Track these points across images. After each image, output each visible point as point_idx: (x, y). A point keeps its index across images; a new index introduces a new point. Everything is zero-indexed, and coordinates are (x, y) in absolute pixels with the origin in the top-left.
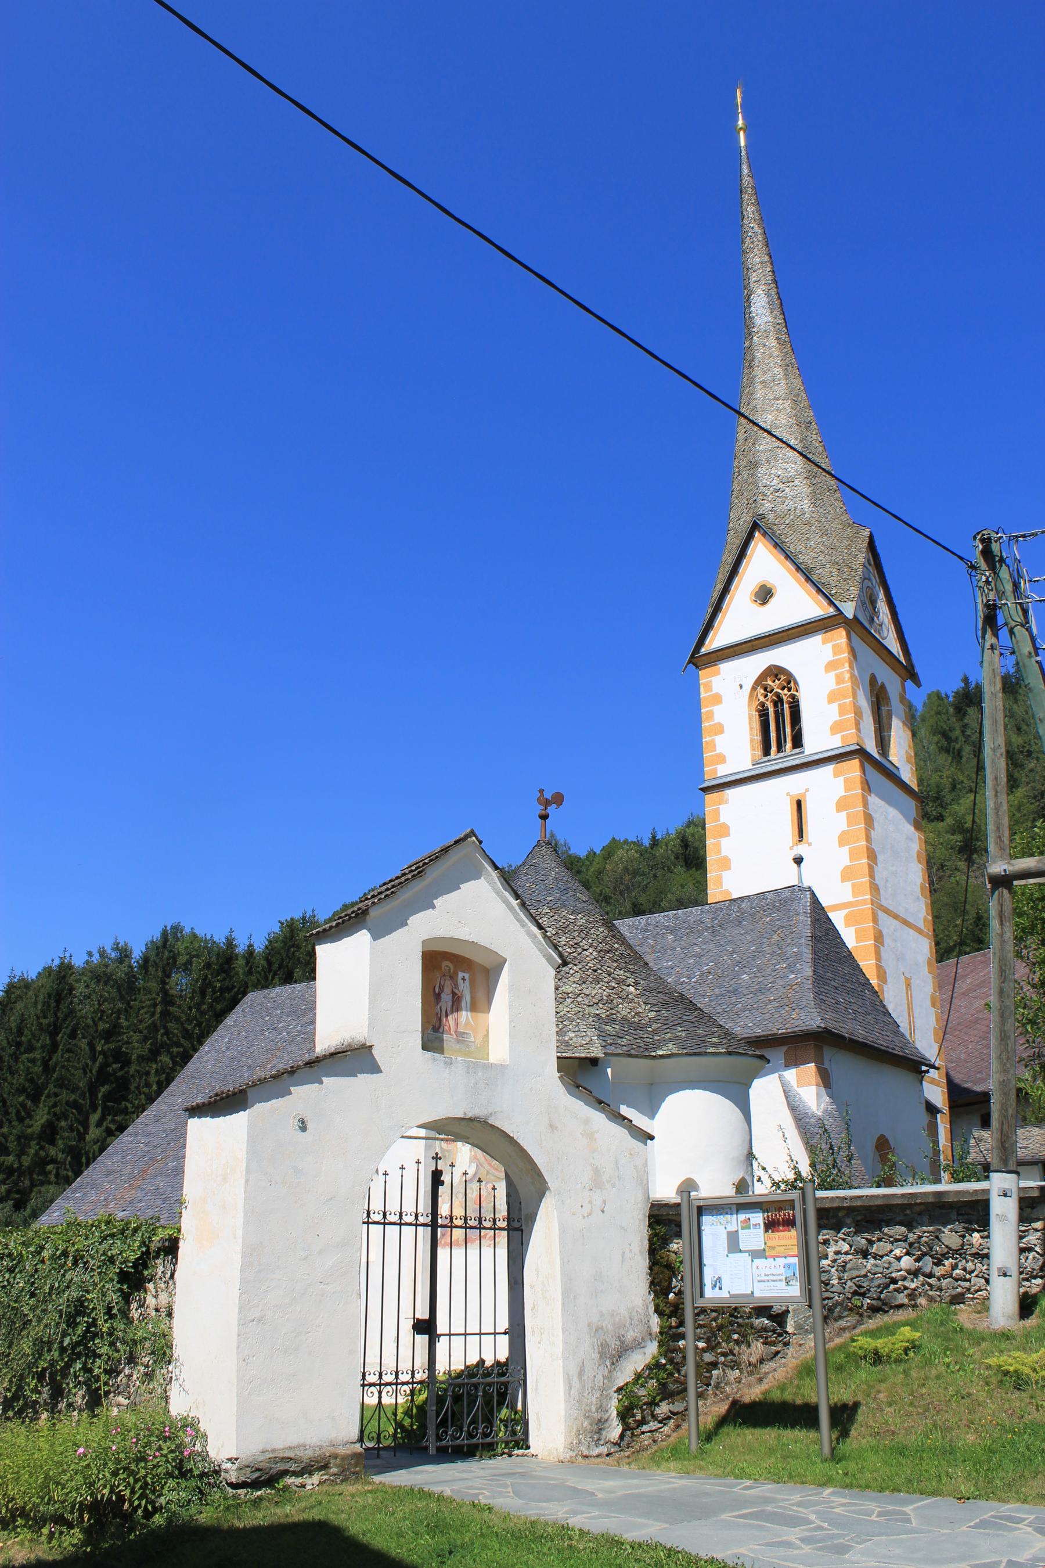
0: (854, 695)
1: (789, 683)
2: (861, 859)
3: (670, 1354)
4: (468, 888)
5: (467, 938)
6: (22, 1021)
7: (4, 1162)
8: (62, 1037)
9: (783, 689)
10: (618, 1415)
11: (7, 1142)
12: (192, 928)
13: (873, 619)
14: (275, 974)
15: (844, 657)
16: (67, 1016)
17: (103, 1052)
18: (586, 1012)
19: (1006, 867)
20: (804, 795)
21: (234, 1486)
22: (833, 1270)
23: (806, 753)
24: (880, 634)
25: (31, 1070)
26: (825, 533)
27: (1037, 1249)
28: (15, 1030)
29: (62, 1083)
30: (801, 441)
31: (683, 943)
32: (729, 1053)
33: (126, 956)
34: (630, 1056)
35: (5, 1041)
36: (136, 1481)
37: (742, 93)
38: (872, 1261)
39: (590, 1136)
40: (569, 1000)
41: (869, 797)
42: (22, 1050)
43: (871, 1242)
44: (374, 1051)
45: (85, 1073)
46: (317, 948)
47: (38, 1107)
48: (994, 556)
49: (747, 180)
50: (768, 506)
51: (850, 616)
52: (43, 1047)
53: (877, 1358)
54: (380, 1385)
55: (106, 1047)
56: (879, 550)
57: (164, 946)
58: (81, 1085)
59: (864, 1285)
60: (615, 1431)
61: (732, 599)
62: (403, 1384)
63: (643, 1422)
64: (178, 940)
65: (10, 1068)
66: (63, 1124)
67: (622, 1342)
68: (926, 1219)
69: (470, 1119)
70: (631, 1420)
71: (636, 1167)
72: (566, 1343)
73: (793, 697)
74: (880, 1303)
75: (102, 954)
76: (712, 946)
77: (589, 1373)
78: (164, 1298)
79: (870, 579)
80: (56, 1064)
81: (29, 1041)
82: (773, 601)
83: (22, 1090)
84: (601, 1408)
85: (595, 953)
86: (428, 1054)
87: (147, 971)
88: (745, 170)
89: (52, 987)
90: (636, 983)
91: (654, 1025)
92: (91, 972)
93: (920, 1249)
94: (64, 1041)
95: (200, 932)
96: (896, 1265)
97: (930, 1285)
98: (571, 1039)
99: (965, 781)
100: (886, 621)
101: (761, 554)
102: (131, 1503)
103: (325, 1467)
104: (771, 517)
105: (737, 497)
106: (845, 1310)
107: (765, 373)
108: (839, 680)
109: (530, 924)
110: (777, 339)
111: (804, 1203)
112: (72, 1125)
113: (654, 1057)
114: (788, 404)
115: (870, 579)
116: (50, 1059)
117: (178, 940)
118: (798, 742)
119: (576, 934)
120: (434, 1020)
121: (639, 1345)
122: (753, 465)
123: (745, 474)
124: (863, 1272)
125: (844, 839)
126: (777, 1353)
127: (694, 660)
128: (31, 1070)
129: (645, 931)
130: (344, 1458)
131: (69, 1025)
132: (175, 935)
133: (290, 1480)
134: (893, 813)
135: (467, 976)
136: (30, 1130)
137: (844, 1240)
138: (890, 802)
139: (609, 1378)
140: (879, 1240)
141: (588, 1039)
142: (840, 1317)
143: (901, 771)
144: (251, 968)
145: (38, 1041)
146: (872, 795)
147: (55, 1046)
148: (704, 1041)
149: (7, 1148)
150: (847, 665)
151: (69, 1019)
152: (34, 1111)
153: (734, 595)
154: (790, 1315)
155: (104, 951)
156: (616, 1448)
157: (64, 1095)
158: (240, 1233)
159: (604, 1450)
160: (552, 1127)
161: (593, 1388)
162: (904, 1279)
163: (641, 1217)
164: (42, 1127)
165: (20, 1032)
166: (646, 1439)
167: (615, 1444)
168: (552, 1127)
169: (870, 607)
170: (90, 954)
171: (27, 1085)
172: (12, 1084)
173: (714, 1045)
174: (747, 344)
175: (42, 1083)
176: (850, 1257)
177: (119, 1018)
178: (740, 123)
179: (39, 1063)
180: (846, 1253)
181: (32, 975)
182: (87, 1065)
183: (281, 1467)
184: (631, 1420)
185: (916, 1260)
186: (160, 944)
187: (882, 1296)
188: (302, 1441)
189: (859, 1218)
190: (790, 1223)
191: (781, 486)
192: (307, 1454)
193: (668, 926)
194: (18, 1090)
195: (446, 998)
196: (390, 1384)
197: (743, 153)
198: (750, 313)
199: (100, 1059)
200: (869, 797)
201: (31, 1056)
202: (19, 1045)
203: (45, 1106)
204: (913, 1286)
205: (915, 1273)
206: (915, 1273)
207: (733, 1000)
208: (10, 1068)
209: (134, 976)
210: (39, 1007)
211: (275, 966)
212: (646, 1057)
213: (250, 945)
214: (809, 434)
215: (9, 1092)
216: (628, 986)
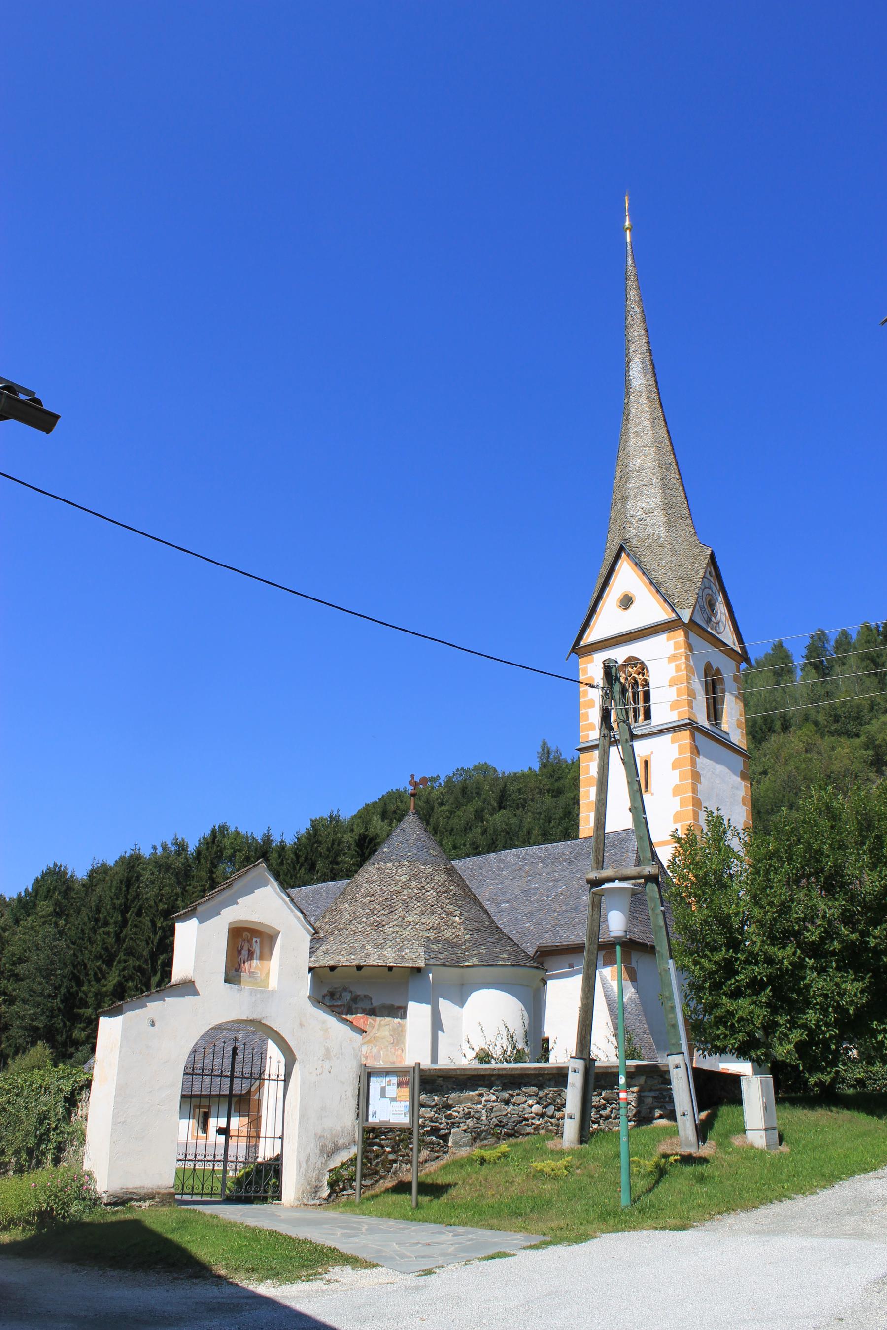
0: (689, 679)
1: (643, 670)
2: (688, 806)
3: (365, 1154)
4: (259, 892)
5: (256, 920)
6: (100, 901)
7: (84, 1013)
8: (131, 915)
9: (638, 675)
10: (328, 1184)
11: (87, 997)
12: (236, 828)
13: (710, 619)
14: (302, 865)
15: (682, 652)
16: (135, 898)
17: (162, 928)
18: (420, 935)
19: (596, 875)
20: (649, 756)
21: (106, 1205)
22: (484, 1111)
23: (652, 725)
24: (716, 630)
25: (106, 941)
26: (675, 553)
27: (633, 1104)
28: (94, 908)
29: (130, 952)
30: (661, 480)
31: (548, 870)
32: (513, 965)
33: (183, 850)
34: (445, 966)
35: (87, 918)
36: (60, 1200)
37: (629, 200)
38: (512, 1107)
39: (326, 1030)
40: (410, 927)
41: (697, 759)
42: (100, 924)
43: (512, 1096)
44: (196, 984)
45: (148, 944)
46: (177, 924)
47: (111, 970)
48: (612, 676)
49: (631, 270)
50: (633, 531)
51: (686, 620)
52: (115, 923)
53: (483, 1161)
54: (195, 1160)
55: (164, 924)
56: (719, 564)
57: (213, 842)
58: (144, 953)
59: (504, 1120)
60: (325, 1192)
61: (604, 603)
62: (189, 1160)
63: (344, 1189)
64: (224, 837)
65: (90, 938)
66: (130, 984)
67: (336, 1145)
68: (553, 1083)
69: (250, 1020)
70: (337, 1188)
71: (354, 1048)
72: (299, 1143)
73: (646, 680)
74: (513, 1132)
75: (164, 847)
76: (567, 873)
77: (313, 1159)
78: (84, 1112)
79: (710, 588)
80: (126, 936)
81: (105, 917)
82: (632, 607)
83: (99, 957)
84: (318, 1180)
85: (434, 893)
86: (228, 985)
87: (199, 862)
88: (630, 262)
89: (123, 875)
90: (461, 914)
91: (468, 944)
92: (156, 862)
93: (546, 1101)
94: (132, 918)
95: (243, 831)
96: (528, 1110)
97: (551, 1123)
98: (406, 954)
99: (882, 704)
100: (724, 619)
101: (625, 568)
102: (57, 1212)
103: (153, 1198)
104: (635, 541)
105: (613, 523)
106: (489, 1135)
107: (637, 425)
108: (678, 669)
109: (296, 911)
110: (648, 397)
111: (414, 1073)
112: (137, 985)
113: (462, 967)
114: (653, 450)
115: (710, 588)
116: (121, 932)
117: (224, 837)
118: (648, 715)
119: (424, 879)
120: (236, 966)
121: (346, 1147)
122: (625, 499)
123: (619, 505)
124: (504, 1113)
125: (676, 791)
126: (437, 1157)
127: (575, 651)
128: (106, 941)
129: (525, 859)
130: (163, 1194)
131: (136, 905)
132: (222, 832)
133: (134, 1203)
134: (720, 768)
135: (258, 940)
136: (104, 989)
137: (494, 1094)
138: (718, 761)
139: (325, 1164)
140: (518, 1094)
141: (417, 954)
142: (485, 1139)
143: (731, 736)
144: (282, 860)
145: (112, 917)
146: (701, 757)
147: (125, 922)
148: (497, 957)
149: (87, 1002)
150: (683, 658)
151: (137, 901)
152: (108, 973)
153: (605, 601)
154: (451, 1136)
155: (166, 845)
156: (326, 1202)
157: (131, 961)
158: (115, 1078)
159: (318, 1202)
160: (301, 1025)
161: (314, 1169)
162: (533, 1118)
163: (354, 1076)
164: (114, 986)
165: (98, 911)
166: (344, 1199)
167: (325, 1200)
168: (301, 1025)
169: (708, 610)
170: (155, 848)
171: (103, 952)
172: (92, 951)
173: (504, 959)
174: (626, 401)
175: (115, 951)
176: (496, 1104)
177: (177, 900)
178: (627, 223)
179: (112, 935)
180: (494, 1102)
181: (111, 863)
182: (149, 938)
183: (129, 1196)
184: (337, 1188)
185: (543, 1108)
186: (209, 841)
187: (516, 1128)
188: (142, 1185)
189: (506, 1081)
190: (407, 1083)
191: (644, 515)
192: (143, 1191)
193: (540, 856)
194: (96, 956)
195: (245, 953)
196: (201, 1161)
197: (629, 248)
198: (629, 376)
199: (160, 933)
200: (697, 759)
201: (107, 929)
202: (97, 920)
203: (117, 970)
204: (538, 1122)
205: (542, 1115)
206: (542, 1115)
207: (573, 915)
208: (90, 938)
209: (189, 866)
210: (113, 891)
211: (302, 859)
212: (456, 967)
213: (282, 842)
214: (668, 473)
215: (89, 958)
216: (455, 916)
